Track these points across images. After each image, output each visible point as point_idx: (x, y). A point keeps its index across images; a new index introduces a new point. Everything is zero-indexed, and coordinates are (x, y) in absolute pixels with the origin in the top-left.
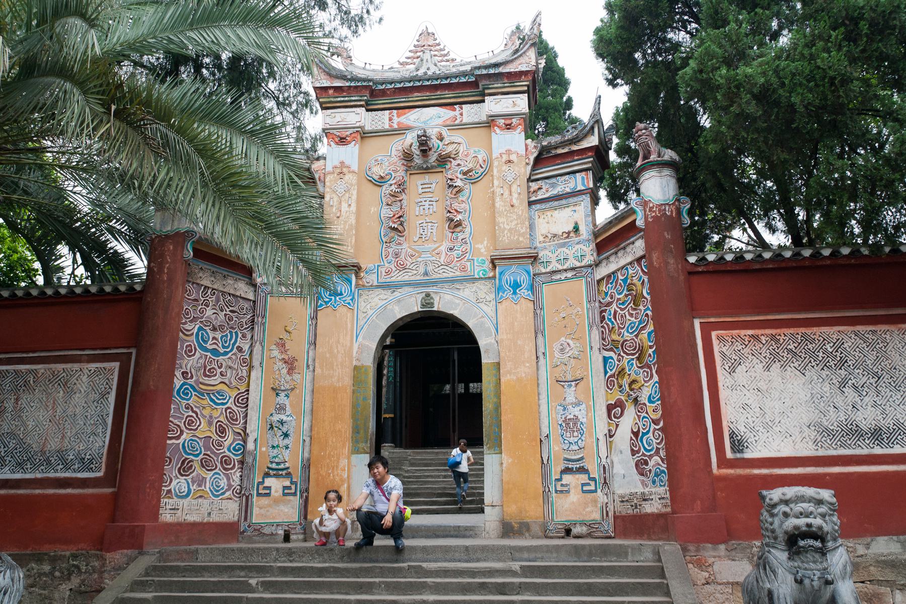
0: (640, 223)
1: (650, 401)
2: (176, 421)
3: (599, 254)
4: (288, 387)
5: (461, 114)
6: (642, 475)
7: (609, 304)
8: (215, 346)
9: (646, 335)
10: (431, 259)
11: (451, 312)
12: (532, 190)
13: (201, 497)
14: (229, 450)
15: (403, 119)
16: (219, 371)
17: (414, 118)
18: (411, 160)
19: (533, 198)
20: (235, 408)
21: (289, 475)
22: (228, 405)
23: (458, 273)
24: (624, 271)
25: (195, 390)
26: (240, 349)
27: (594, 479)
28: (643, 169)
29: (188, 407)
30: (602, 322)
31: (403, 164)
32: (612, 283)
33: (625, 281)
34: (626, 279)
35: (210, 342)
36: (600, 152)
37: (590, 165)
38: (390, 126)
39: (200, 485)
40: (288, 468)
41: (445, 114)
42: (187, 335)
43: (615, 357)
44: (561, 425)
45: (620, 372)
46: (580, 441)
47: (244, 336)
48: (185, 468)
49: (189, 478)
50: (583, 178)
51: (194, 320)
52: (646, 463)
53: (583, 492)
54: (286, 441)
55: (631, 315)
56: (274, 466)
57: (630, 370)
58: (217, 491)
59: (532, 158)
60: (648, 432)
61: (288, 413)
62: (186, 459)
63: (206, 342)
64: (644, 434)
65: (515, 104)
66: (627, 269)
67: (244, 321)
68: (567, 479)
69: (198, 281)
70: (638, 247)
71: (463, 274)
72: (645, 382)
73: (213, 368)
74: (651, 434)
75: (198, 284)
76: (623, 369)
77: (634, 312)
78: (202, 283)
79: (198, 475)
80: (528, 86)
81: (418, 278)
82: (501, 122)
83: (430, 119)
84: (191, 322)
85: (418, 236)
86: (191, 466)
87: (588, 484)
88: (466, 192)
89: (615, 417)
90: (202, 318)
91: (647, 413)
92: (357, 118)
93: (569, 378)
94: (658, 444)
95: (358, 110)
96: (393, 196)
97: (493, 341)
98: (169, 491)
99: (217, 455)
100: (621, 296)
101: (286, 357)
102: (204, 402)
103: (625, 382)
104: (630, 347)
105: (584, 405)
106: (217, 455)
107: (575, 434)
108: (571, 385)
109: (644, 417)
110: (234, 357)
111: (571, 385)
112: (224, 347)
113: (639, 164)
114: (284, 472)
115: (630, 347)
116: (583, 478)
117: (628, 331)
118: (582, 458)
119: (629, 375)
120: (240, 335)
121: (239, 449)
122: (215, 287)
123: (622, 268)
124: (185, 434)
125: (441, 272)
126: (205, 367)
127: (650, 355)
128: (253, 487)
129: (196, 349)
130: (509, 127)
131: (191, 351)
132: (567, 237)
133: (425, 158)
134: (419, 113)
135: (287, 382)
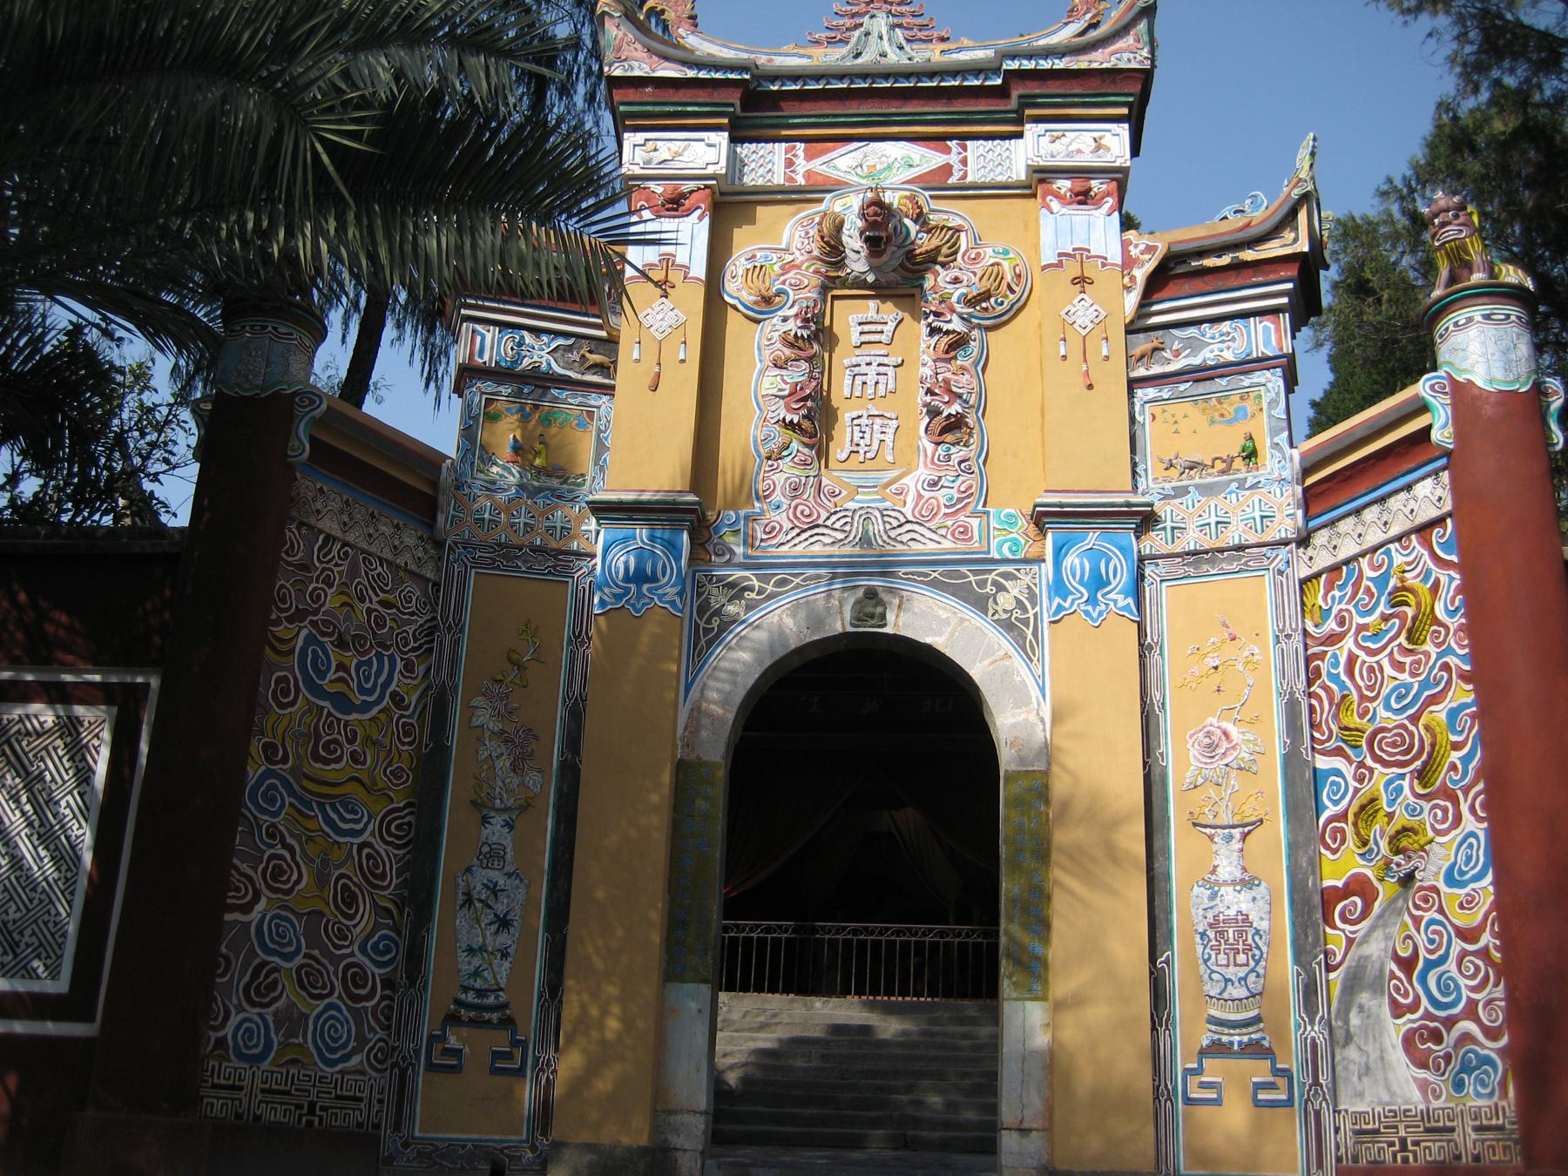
0: (1442, 435)
1: (1450, 880)
2: (244, 867)
3: (1308, 517)
4: (510, 803)
5: (964, 162)
6: (1423, 1065)
7: (1333, 639)
8: (340, 687)
9: (1443, 716)
10: (881, 505)
11: (928, 640)
12: (1137, 351)
13: (294, 1062)
14: (363, 949)
15: (817, 165)
16: (348, 748)
17: (844, 161)
18: (840, 264)
19: (1141, 372)
20: (381, 847)
21: (507, 1023)
22: (365, 837)
23: (947, 544)
24: (1379, 556)
25: (291, 792)
26: (397, 699)
27: (1286, 1073)
28: (1444, 308)
29: (273, 832)
30: (1309, 684)
31: (816, 272)
32: (1342, 588)
33: (1382, 581)
34: (1385, 578)
35: (331, 676)
36: (1308, 266)
37: (1285, 300)
38: (965, 148)
39: (291, 1033)
40: (505, 1006)
41: (926, 159)
42: (279, 653)
43: (1348, 771)
44: (1203, 935)
45: (1363, 808)
46: (1252, 978)
47: (409, 667)
48: (261, 989)
49: (269, 1013)
50: (1266, 329)
51: (299, 616)
52: (1437, 1037)
53: (1257, 1104)
54: (504, 939)
55: (1399, 667)
56: (470, 997)
57: (1391, 803)
58: (333, 1051)
59: (1141, 274)
60: (1443, 959)
61: (509, 868)
62: (264, 963)
63: (322, 675)
64: (1430, 965)
65: (1098, 145)
66: (1388, 553)
67: (411, 629)
68: (1214, 1070)
69: (312, 521)
70: (1429, 495)
71: (961, 546)
72: (1438, 833)
73: (335, 741)
74: (1451, 965)
75: (311, 527)
76: (1373, 800)
77: (1408, 660)
78: (320, 525)
79: (291, 1005)
80: (1129, 105)
81: (848, 550)
82: (1064, 185)
83: (890, 165)
84: (290, 620)
85: (848, 448)
86: (275, 982)
87: (1270, 1086)
88: (974, 346)
89: (1345, 920)
90: (316, 612)
91: (1441, 911)
92: (711, 155)
93: (1225, 819)
94: (1474, 989)
95: (713, 137)
96: (792, 345)
97: (1032, 718)
98: (221, 1042)
99: (336, 961)
100: (1367, 620)
101: (510, 728)
102: (311, 825)
103: (1378, 831)
104: (1394, 744)
105: (1262, 888)
106: (336, 961)
107: (1241, 958)
108: (1231, 837)
109: (1432, 922)
110: (383, 717)
111: (1231, 837)
112: (362, 691)
113: (1437, 293)
114: (495, 1016)
115: (1394, 744)
116: (1259, 1071)
117: (1388, 707)
118: (1257, 1020)
119: (1390, 816)
120: (400, 665)
121: (388, 950)
122: (350, 538)
123: (1375, 549)
124: (263, 901)
125: (905, 538)
126: (318, 737)
127: (1453, 767)
128: (417, 1052)
129: (298, 690)
130: (1083, 197)
131: (286, 693)
132: (1223, 472)
133: (896, 261)
134: (858, 155)
135: (509, 791)
